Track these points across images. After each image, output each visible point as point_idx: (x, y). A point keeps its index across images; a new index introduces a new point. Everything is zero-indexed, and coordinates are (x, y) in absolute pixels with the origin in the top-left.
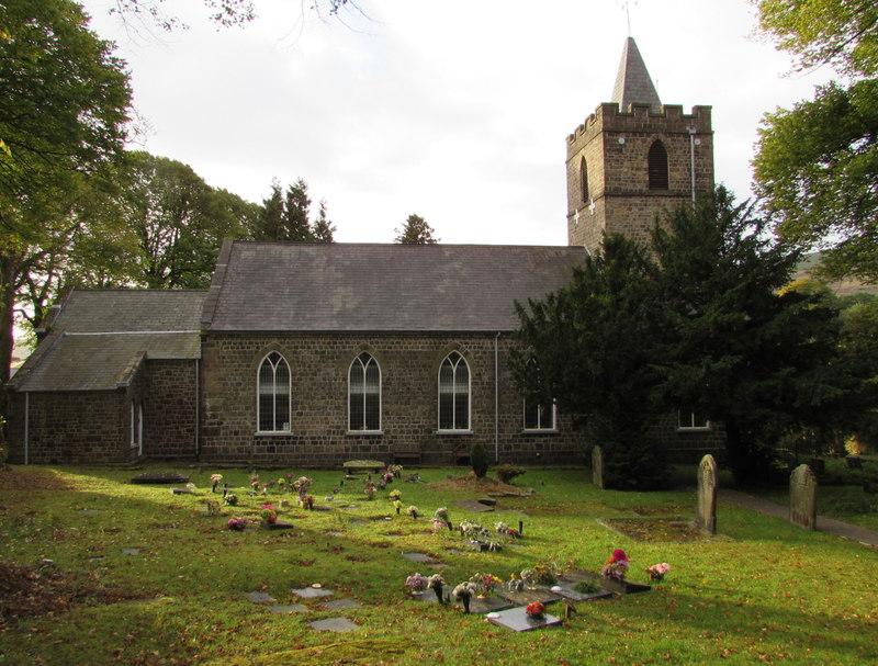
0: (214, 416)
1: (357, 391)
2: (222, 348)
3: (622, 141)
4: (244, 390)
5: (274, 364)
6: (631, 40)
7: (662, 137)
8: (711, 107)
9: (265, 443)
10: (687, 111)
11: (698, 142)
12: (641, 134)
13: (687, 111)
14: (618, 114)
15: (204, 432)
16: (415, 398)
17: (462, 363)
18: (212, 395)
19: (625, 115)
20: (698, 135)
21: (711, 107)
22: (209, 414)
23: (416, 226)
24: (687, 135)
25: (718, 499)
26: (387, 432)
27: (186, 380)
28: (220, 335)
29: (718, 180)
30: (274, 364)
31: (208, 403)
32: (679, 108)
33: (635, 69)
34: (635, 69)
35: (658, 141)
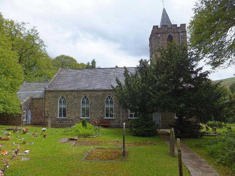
0: (47, 113)
1: (107, 106)
2: (50, 95)
3: (159, 36)
4: (55, 106)
5: (85, 99)
6: (164, 9)
7: (171, 34)
8: (185, 24)
9: (59, 121)
10: (179, 26)
11: (182, 34)
12: (165, 33)
13: (179, 26)
14: (158, 29)
15: (45, 117)
16: (99, 109)
17: (111, 98)
18: (47, 107)
19: (160, 29)
20: (182, 32)
21: (185, 24)
22: (46, 112)
23: (94, 62)
24: (179, 33)
25: (126, 139)
26: (91, 118)
27: (41, 103)
28: (49, 91)
29: (79, 63)
30: (85, 99)
31: (46, 109)
32: (176, 25)
33: (165, 16)
34: (165, 16)
35: (170, 35)
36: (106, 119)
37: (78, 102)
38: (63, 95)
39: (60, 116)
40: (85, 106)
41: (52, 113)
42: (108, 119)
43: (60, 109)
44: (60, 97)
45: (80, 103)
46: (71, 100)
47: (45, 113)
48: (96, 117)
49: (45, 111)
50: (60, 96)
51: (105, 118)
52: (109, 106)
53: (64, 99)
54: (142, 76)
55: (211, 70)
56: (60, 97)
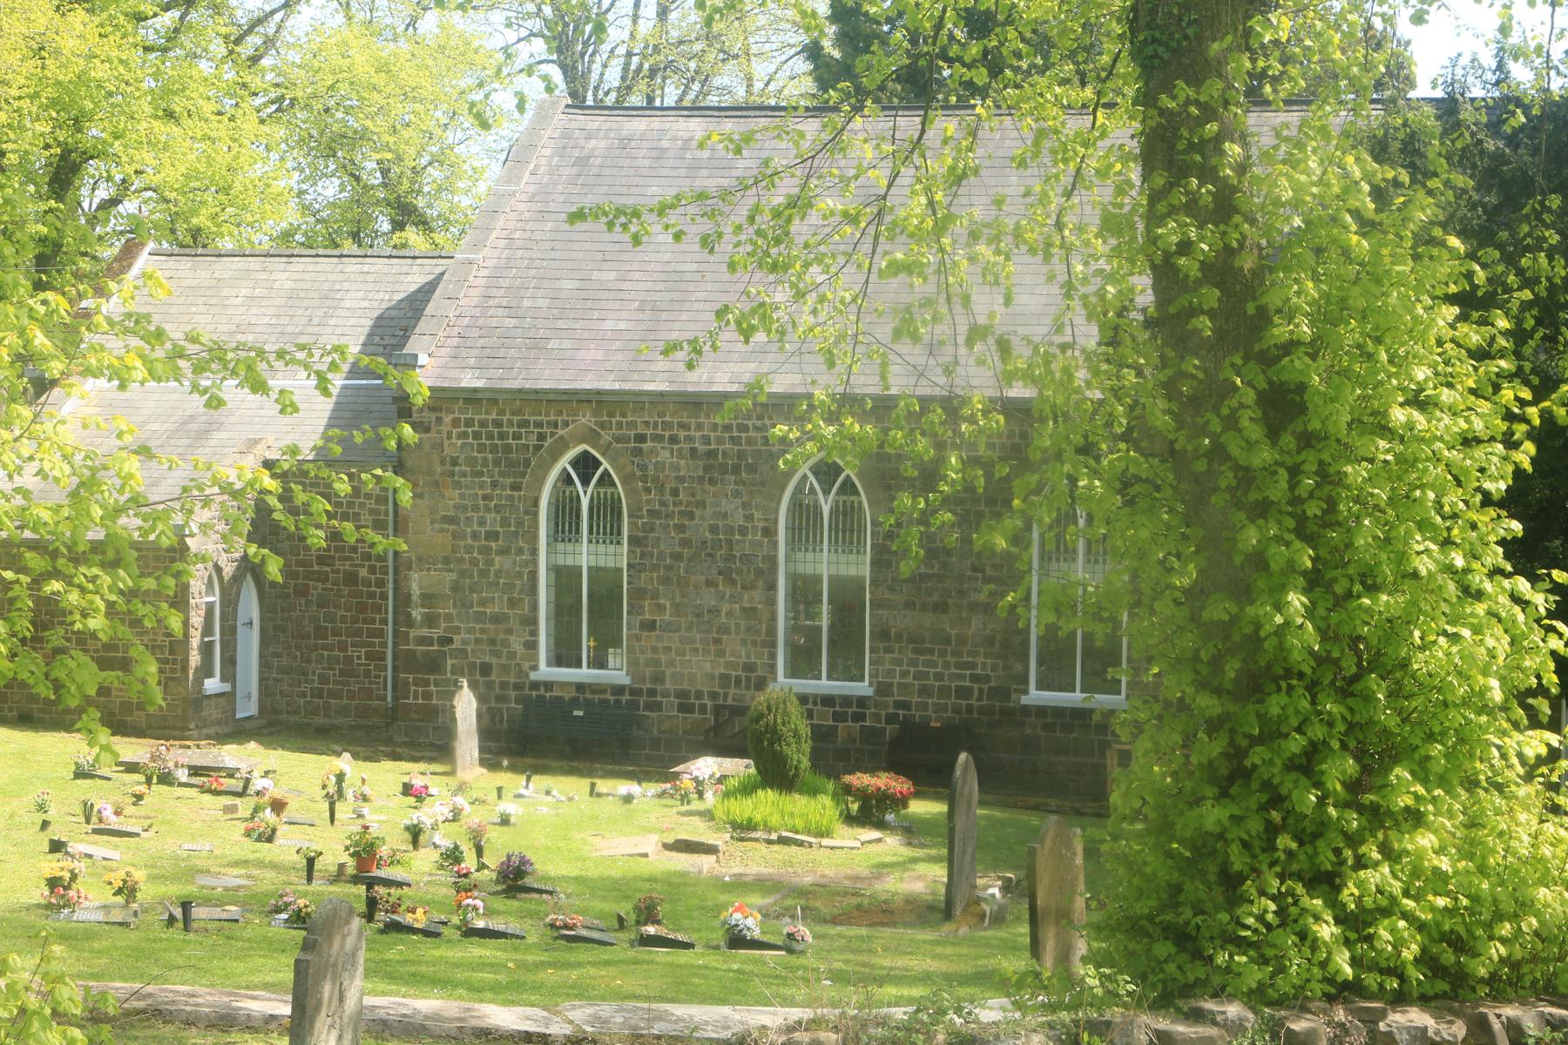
0: (430, 621)
22: (417, 614)
36: (1041, 711)
37: (749, 518)
38: (592, 437)
39: (565, 655)
40: (585, 555)
41: (480, 617)
42: (1058, 712)
43: (565, 578)
44: (564, 462)
45: (769, 532)
46: (675, 492)
47: (406, 620)
48: (939, 677)
49: (403, 600)
50: (555, 456)
51: (1036, 696)
52: (585, 555)
53: (849, 488)
54: (331, 463)
55: (1299, 459)
56: (564, 462)
